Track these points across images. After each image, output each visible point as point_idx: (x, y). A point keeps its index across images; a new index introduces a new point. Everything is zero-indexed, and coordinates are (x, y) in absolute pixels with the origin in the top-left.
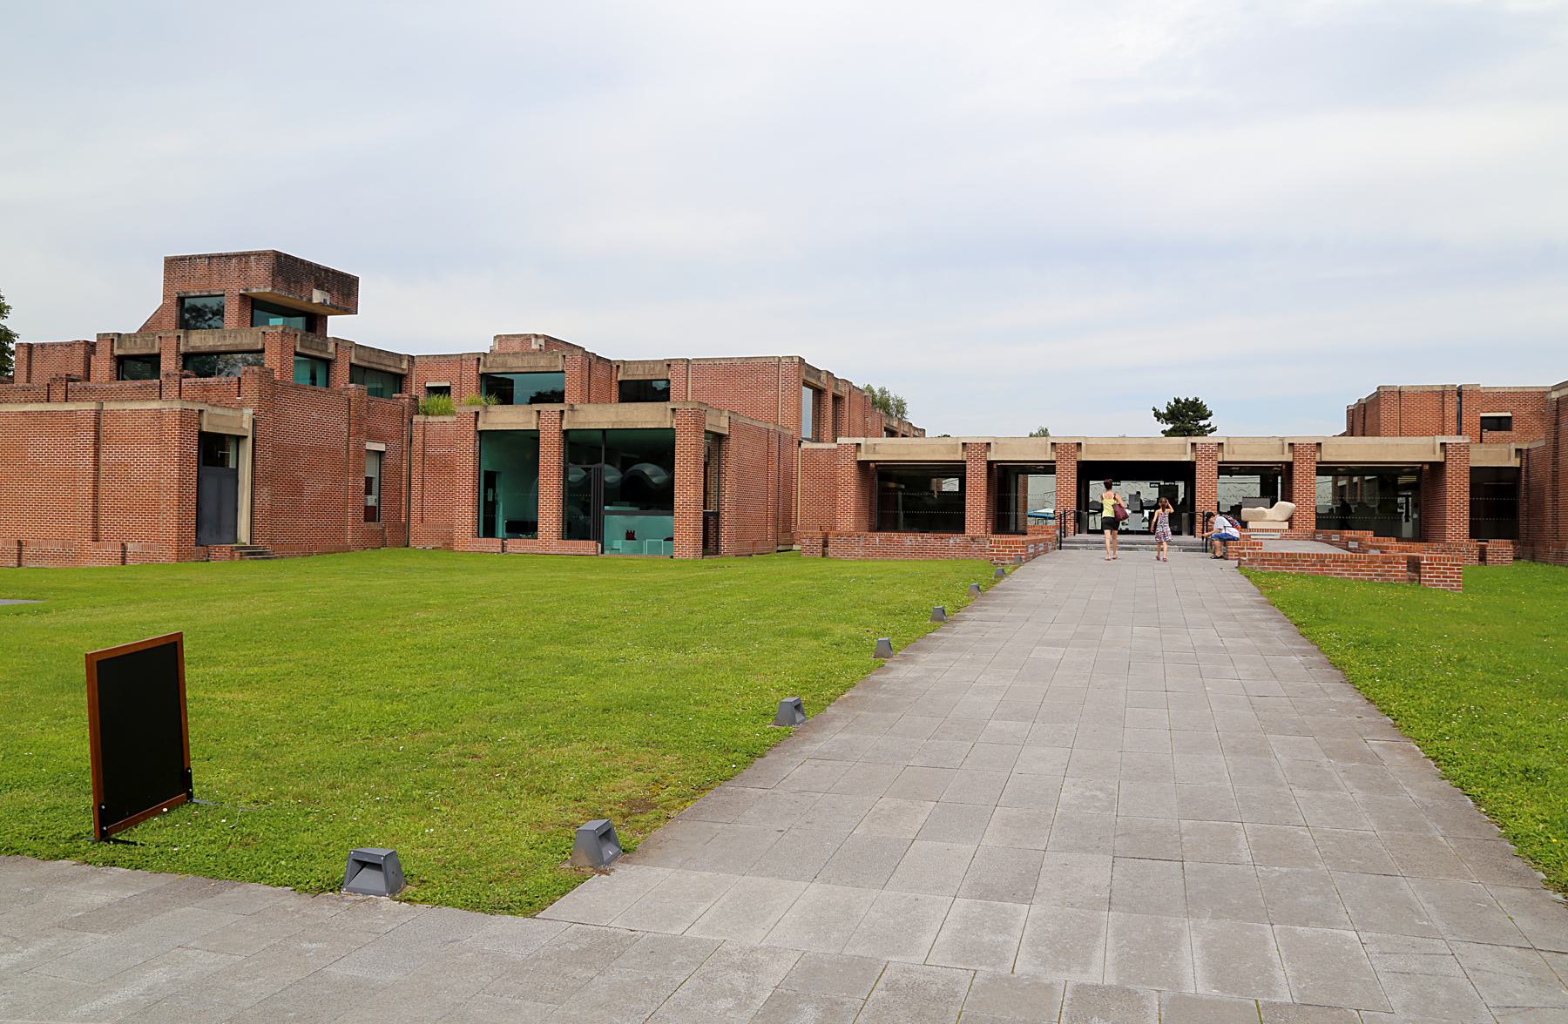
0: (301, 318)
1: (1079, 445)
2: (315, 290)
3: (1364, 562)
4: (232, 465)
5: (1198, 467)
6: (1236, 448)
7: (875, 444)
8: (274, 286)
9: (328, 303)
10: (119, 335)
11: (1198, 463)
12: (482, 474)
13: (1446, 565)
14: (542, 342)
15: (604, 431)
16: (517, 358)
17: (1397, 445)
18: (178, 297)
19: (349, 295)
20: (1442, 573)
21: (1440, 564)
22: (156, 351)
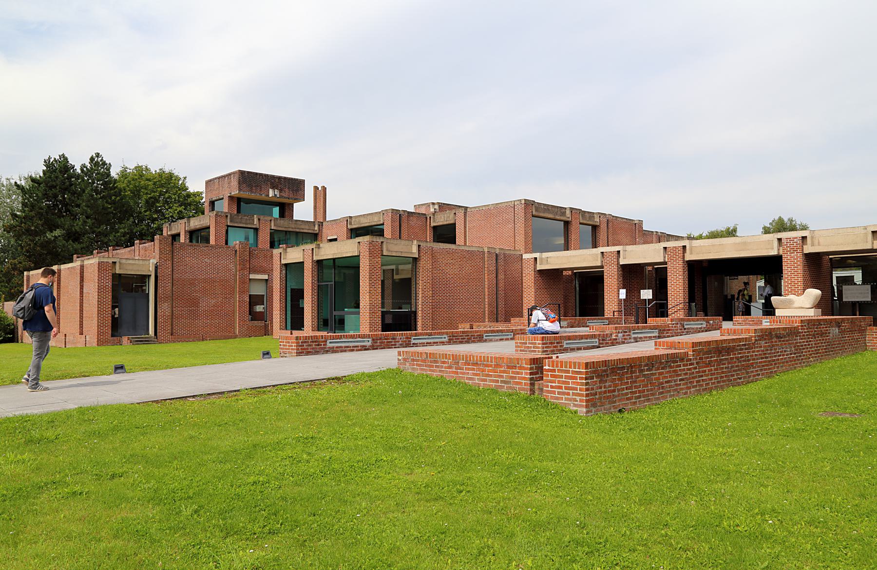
2: (270, 190)
3: (491, 366)
4: (147, 292)
5: (784, 260)
7: (547, 257)
8: (240, 190)
9: (278, 196)
10: (351, 217)
12: (289, 294)
13: (568, 372)
14: (437, 207)
15: (334, 259)
16: (365, 217)
18: (210, 201)
19: (297, 191)
20: (564, 382)
21: (562, 371)
22: (452, 222)
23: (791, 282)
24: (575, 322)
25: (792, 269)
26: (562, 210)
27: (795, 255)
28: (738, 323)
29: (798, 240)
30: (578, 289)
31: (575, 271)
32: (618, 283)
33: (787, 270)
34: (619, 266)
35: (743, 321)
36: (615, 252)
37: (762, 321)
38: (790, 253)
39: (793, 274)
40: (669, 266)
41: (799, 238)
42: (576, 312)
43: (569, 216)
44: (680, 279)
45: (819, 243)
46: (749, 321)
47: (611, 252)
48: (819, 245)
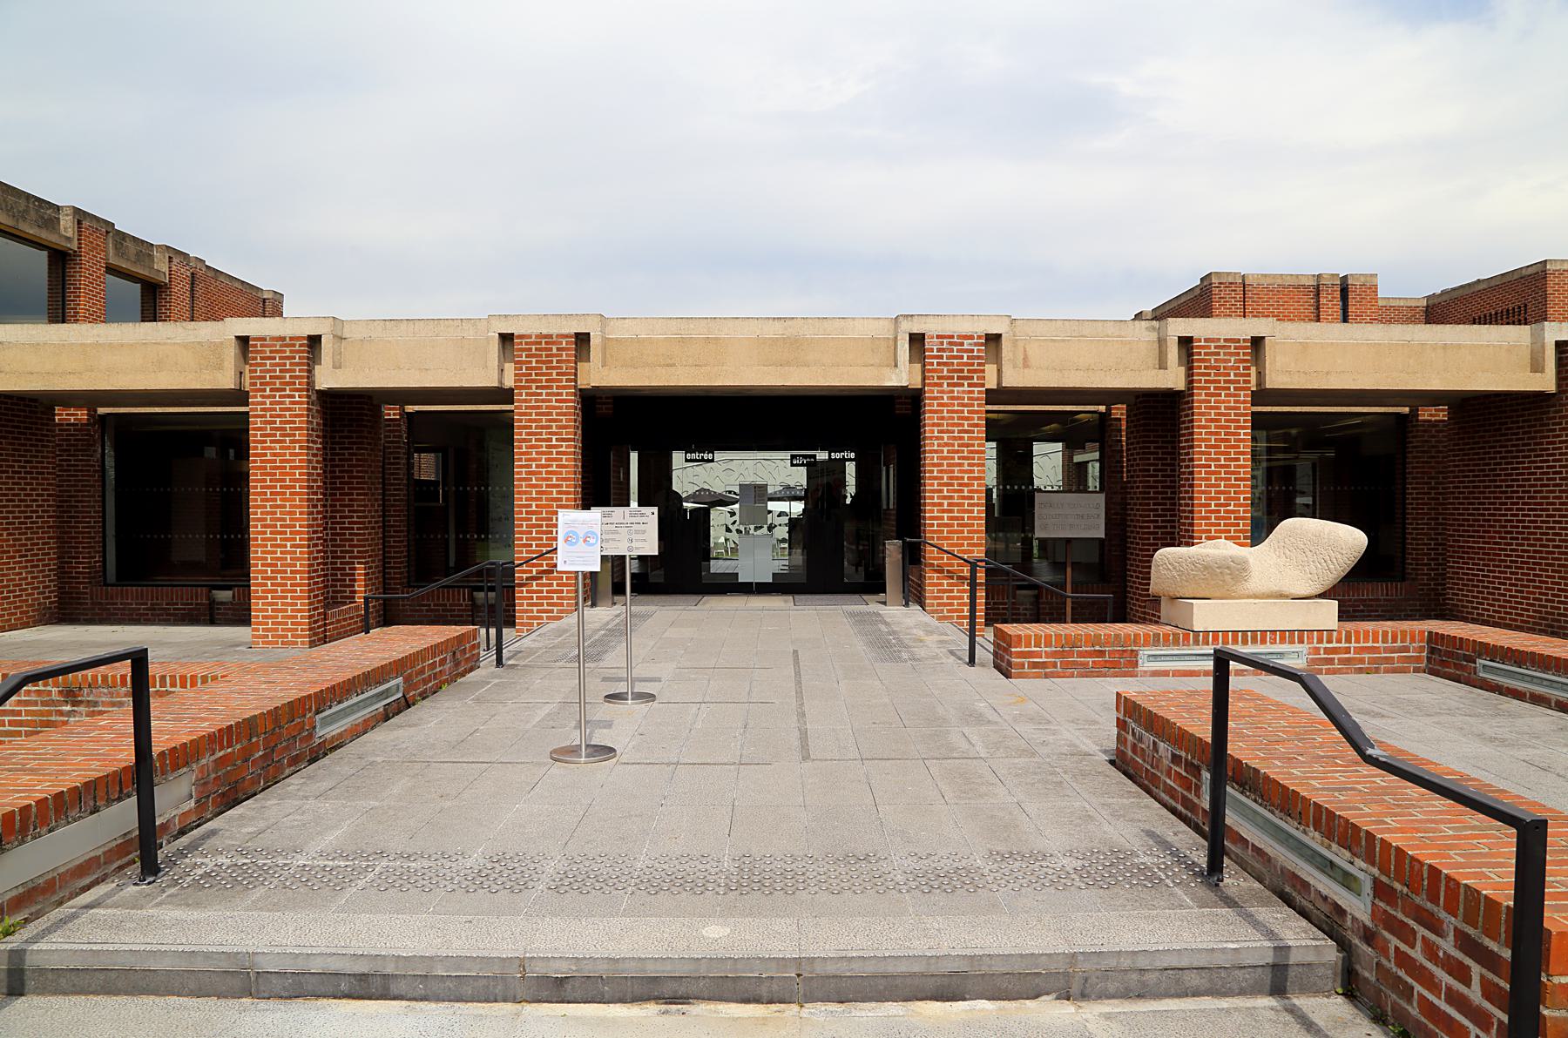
0: (1097, 560)
1: (582, 340)
5: (930, 405)
6: (1034, 351)
11: (931, 392)
17: (1445, 347)
23: (951, 478)
24: (246, 755)
25: (955, 438)
26: (45, 211)
27: (964, 392)
28: (1034, 665)
29: (976, 344)
30: (111, 473)
31: (101, 411)
32: (309, 461)
33: (937, 438)
34: (314, 397)
35: (1054, 654)
36: (298, 338)
37: (1134, 653)
38: (948, 385)
39: (958, 452)
40: (520, 409)
41: (979, 337)
42: (104, 557)
43: (69, 234)
44: (564, 453)
45: (1025, 359)
46: (1081, 655)
47: (282, 339)
48: (1026, 364)
